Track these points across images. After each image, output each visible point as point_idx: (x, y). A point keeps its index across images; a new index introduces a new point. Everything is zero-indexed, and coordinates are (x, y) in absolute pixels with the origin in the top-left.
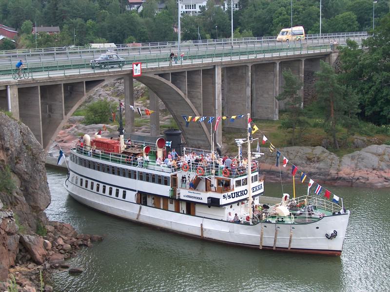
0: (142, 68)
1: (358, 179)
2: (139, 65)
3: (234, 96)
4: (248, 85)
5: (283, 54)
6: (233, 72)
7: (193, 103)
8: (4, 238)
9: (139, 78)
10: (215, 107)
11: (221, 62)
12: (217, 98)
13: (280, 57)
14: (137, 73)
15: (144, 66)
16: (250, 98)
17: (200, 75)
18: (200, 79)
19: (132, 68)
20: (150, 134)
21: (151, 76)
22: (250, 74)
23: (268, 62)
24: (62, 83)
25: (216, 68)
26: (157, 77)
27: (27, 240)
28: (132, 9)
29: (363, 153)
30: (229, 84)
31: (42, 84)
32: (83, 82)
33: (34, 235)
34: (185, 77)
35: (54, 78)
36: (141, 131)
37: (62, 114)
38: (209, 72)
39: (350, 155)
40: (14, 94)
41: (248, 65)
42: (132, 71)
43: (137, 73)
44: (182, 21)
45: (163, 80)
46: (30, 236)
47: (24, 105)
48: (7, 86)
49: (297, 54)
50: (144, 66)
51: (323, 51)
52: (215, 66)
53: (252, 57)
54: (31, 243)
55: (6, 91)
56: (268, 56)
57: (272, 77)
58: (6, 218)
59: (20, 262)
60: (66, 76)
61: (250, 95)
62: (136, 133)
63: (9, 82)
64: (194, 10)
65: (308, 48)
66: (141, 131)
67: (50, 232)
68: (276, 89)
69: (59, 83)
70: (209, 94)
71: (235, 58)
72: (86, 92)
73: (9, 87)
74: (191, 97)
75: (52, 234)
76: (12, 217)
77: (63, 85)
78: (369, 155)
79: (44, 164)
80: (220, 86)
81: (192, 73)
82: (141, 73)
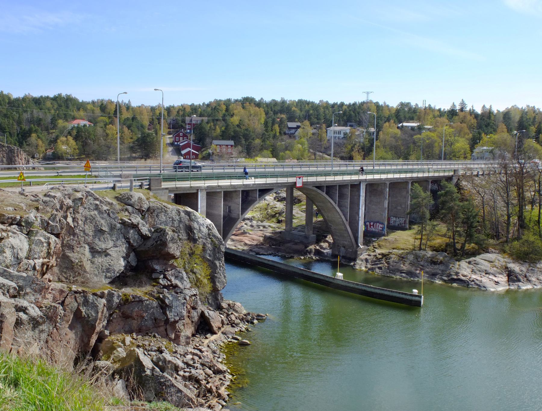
0: (303, 181)
1: (473, 281)
2: (301, 178)
3: (374, 206)
4: (386, 198)
5: (415, 175)
6: (372, 186)
7: (341, 210)
8: (189, 311)
9: (299, 189)
10: (359, 215)
11: (366, 180)
12: (361, 208)
13: (412, 177)
14: (299, 184)
15: (305, 179)
16: (387, 209)
17: (348, 189)
18: (348, 192)
19: (295, 181)
20: (304, 233)
21: (310, 187)
22: (388, 190)
23: (402, 181)
24: (241, 189)
25: (362, 184)
26: (315, 189)
27: (207, 314)
28: (290, 132)
29: (478, 259)
30: (370, 196)
31: (225, 190)
32: (257, 190)
33: (213, 310)
34: (336, 189)
35: (234, 186)
36: (297, 230)
37: (239, 214)
38: (355, 186)
39: (468, 260)
40: (203, 197)
41: (409, 181)
42: (295, 183)
43: (299, 184)
44: (400, 158)
45: (319, 191)
46: (209, 312)
47: (210, 206)
48: (198, 190)
49: (415, 176)
50: (305, 179)
51: (446, 174)
52: (360, 182)
53: (390, 176)
54: (209, 317)
55: (197, 193)
56: (403, 176)
57: (404, 193)
58: (192, 295)
59: (200, 332)
60: (244, 185)
61: (387, 206)
62: (293, 231)
63: (199, 187)
64: (339, 135)
65: (435, 171)
66: (297, 230)
67: (224, 308)
68: (408, 203)
69: (238, 189)
70: (355, 205)
71: (377, 177)
72: (259, 198)
73: (199, 190)
74: (339, 206)
75: (226, 311)
76: (197, 295)
77: (223, 193)
78: (482, 261)
79: (57, 291)
80: (364, 198)
81: (342, 186)
82: (303, 185)
